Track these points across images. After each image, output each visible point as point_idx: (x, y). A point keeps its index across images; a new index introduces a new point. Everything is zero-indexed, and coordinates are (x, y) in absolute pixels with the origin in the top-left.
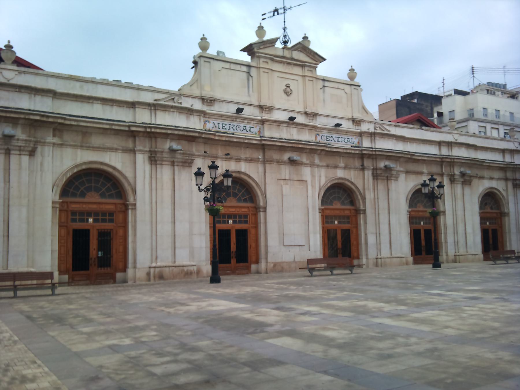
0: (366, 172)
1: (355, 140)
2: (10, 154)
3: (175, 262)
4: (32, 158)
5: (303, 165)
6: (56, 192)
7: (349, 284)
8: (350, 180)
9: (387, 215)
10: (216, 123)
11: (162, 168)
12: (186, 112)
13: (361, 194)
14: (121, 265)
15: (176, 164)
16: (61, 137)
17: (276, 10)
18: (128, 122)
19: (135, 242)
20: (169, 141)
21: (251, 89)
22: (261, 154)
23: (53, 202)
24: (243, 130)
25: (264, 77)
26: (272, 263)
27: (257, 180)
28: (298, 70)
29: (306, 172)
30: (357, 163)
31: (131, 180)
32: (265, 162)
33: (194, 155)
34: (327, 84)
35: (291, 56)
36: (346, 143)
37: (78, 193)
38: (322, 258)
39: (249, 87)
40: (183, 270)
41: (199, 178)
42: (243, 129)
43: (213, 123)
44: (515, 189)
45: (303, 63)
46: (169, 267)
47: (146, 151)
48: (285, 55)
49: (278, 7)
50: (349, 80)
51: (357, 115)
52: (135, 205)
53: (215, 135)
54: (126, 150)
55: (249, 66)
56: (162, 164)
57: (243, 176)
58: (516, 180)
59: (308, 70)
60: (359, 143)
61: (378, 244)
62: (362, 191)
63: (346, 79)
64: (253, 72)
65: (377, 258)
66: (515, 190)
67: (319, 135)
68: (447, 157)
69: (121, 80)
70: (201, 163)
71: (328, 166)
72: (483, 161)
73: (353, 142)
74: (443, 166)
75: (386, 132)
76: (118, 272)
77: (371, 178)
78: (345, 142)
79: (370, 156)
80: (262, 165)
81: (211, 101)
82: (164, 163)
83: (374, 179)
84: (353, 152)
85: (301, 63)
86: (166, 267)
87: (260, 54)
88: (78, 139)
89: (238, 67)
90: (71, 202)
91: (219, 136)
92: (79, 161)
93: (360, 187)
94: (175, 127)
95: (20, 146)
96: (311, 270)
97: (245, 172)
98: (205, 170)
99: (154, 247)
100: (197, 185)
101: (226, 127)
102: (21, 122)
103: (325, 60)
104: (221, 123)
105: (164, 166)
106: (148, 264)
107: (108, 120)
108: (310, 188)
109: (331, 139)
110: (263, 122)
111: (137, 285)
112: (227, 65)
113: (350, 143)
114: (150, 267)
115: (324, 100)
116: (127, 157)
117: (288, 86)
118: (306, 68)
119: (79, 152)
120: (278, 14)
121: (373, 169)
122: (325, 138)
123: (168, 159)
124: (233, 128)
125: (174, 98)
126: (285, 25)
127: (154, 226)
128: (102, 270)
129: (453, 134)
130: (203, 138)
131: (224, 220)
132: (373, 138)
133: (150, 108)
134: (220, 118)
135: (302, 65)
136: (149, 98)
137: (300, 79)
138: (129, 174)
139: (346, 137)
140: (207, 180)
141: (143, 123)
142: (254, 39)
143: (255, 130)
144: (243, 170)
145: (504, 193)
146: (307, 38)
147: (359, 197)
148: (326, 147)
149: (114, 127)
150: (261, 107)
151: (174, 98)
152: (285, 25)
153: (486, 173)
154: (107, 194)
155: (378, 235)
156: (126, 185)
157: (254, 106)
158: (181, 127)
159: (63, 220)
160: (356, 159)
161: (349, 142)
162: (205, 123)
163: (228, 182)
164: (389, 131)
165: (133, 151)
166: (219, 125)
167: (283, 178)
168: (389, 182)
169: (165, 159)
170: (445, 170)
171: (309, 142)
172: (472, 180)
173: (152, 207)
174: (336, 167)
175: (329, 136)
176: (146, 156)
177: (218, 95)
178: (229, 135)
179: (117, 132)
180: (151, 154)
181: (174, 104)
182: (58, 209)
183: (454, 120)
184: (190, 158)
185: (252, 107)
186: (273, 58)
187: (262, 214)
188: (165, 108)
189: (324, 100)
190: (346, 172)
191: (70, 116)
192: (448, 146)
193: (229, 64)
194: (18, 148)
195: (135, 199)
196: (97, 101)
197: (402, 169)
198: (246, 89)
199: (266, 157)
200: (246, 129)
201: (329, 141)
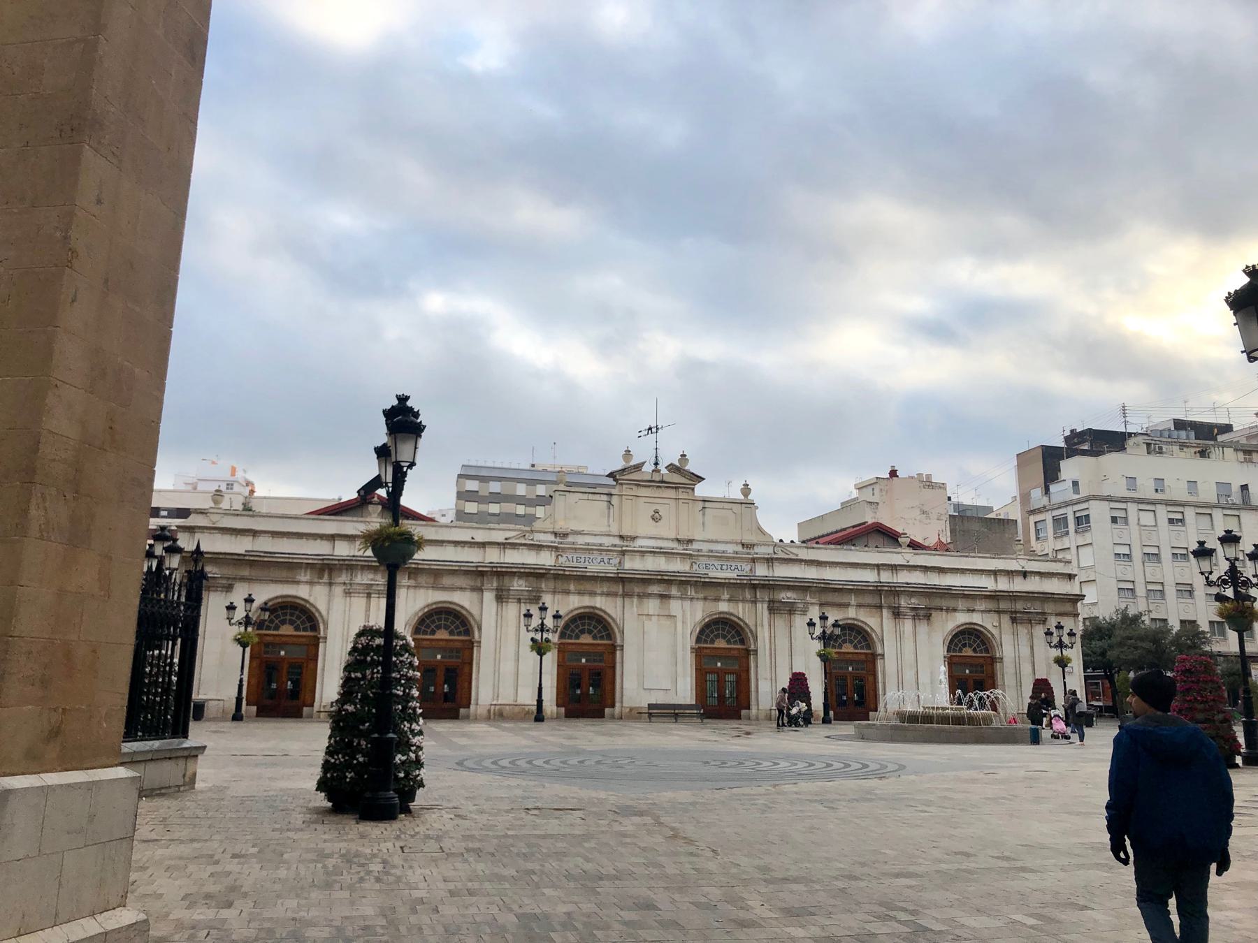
2: (370, 597)
3: (516, 701)
6: (408, 630)
7: (1241, 740)
8: (737, 614)
10: (570, 557)
11: (507, 606)
14: (872, 706)
15: (522, 601)
17: (650, 429)
21: (611, 519)
22: (621, 587)
23: (945, 657)
25: (627, 504)
27: (614, 616)
28: (671, 493)
29: (675, 606)
31: (477, 617)
33: (543, 591)
34: (707, 504)
37: (429, 631)
38: (694, 703)
39: (609, 517)
40: (524, 709)
44: (1015, 624)
46: (509, 705)
47: (493, 589)
48: (653, 479)
51: (748, 538)
52: (480, 642)
53: (564, 570)
54: (474, 589)
56: (507, 602)
57: (597, 612)
65: (771, 710)
66: (500, 606)
67: (696, 563)
70: (1052, 622)
71: (705, 599)
72: (949, 588)
76: (607, 707)
77: (766, 613)
79: (764, 587)
82: (510, 600)
83: (770, 613)
84: (738, 582)
85: (674, 486)
87: (622, 482)
91: (569, 571)
94: (523, 564)
95: (378, 590)
96: (650, 715)
99: (496, 685)
100: (810, 634)
102: (517, 574)
103: (703, 479)
105: (510, 604)
106: (489, 702)
108: (679, 625)
109: (712, 567)
110: (623, 553)
111: (476, 719)
114: (491, 705)
115: (703, 524)
116: (475, 595)
121: (769, 601)
123: (364, 591)
128: (447, 705)
130: (346, 565)
132: (770, 564)
135: (676, 487)
137: (672, 503)
138: (475, 611)
139: (733, 565)
141: (491, 563)
143: (615, 561)
144: (598, 605)
145: (995, 631)
147: (749, 634)
149: (462, 568)
153: (961, 604)
154: (598, 636)
155: (774, 682)
156: (472, 622)
157: (614, 536)
159: (561, 660)
161: (602, 563)
163: (838, 631)
164: (797, 555)
165: (480, 590)
167: (646, 613)
168: (792, 617)
169: (511, 597)
170: (885, 602)
171: (678, 572)
172: (541, 597)
174: (717, 599)
176: (765, 606)
178: (310, 557)
184: (538, 594)
185: (611, 538)
187: (618, 653)
189: (703, 524)
192: (892, 570)
193: (599, 495)
194: (377, 592)
195: (480, 637)
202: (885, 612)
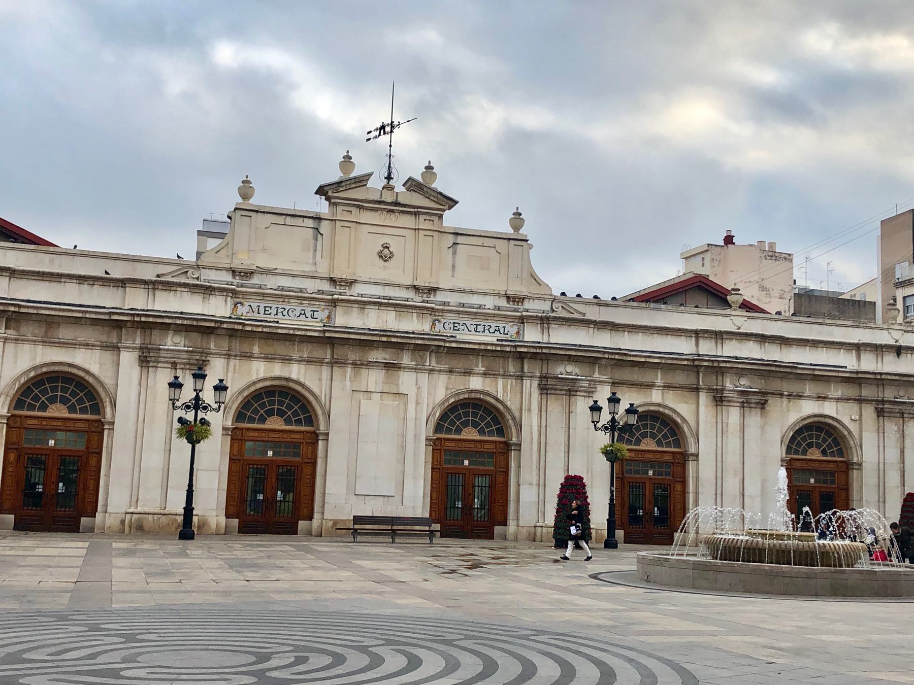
0: (527, 382)
1: (512, 330)
4: (763, 410)
5: (402, 370)
9: (562, 455)
10: (254, 305)
12: (203, 291)
13: (514, 418)
16: (17, 329)
17: (383, 127)
18: (108, 308)
19: (108, 476)
20: (171, 333)
22: (329, 351)
24: (299, 316)
26: (331, 520)
28: (408, 221)
29: (407, 381)
30: (512, 368)
32: (333, 363)
34: (460, 239)
35: (395, 199)
36: (491, 334)
41: (596, 414)
42: (301, 314)
43: (250, 306)
45: (416, 210)
47: (136, 348)
48: (383, 199)
49: (386, 123)
50: (512, 231)
51: (516, 289)
54: (105, 347)
55: (318, 219)
57: (292, 385)
58: (883, 402)
59: (425, 220)
60: (518, 333)
61: (541, 504)
62: (517, 414)
63: (509, 230)
64: (325, 227)
67: (439, 321)
68: (710, 358)
69: (376, 253)
72: (794, 366)
73: (506, 333)
74: (701, 375)
75: (576, 316)
77: (536, 393)
78: (490, 333)
79: (534, 356)
80: (330, 369)
81: (247, 273)
82: (160, 365)
85: (412, 210)
86: (148, 514)
87: (337, 201)
88: (40, 331)
89: (299, 221)
90: (26, 417)
92: (39, 361)
93: (514, 407)
97: (298, 379)
98: (604, 403)
101: (270, 311)
104: (262, 306)
107: (80, 306)
108: (411, 406)
109: (462, 328)
110: (334, 303)
112: (281, 220)
113: (501, 334)
114: (127, 513)
115: (453, 266)
116: (108, 356)
117: (384, 246)
118: (422, 217)
119: (39, 348)
120: (384, 133)
122: (452, 326)
124: (282, 312)
125: (187, 271)
126: (390, 150)
127: (137, 454)
129: (732, 318)
131: (278, 451)
133: (147, 287)
134: (262, 298)
135: (415, 212)
136: (148, 273)
137: (410, 234)
138: (108, 381)
140: (605, 417)
142: (335, 175)
143: (322, 315)
146: (432, 168)
148: (444, 341)
149: (88, 316)
150: (332, 281)
151: (187, 271)
152: (390, 150)
153: (809, 389)
157: (322, 279)
158: (191, 314)
160: (510, 360)
161: (497, 333)
162: (235, 307)
163: (633, 419)
164: (584, 314)
165: (116, 348)
166: (259, 309)
170: (703, 382)
173: (137, 428)
174: (468, 373)
175: (459, 323)
176: (535, 383)
177: (263, 262)
179: (95, 322)
180: (143, 353)
181: (188, 281)
182: (5, 425)
183: (739, 292)
186: (378, 205)
188: (169, 286)
190: (488, 380)
191: (28, 301)
195: (114, 416)
196: (130, 279)
197: (604, 378)
198: (311, 253)
199: (335, 357)
200: (305, 314)
201: (458, 330)
202: (703, 397)
